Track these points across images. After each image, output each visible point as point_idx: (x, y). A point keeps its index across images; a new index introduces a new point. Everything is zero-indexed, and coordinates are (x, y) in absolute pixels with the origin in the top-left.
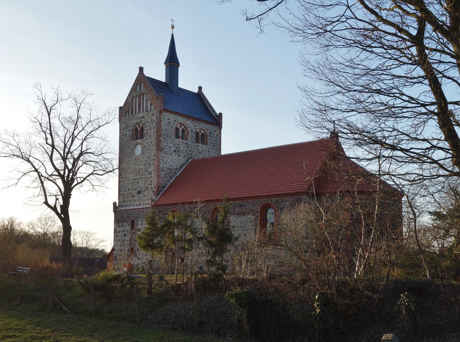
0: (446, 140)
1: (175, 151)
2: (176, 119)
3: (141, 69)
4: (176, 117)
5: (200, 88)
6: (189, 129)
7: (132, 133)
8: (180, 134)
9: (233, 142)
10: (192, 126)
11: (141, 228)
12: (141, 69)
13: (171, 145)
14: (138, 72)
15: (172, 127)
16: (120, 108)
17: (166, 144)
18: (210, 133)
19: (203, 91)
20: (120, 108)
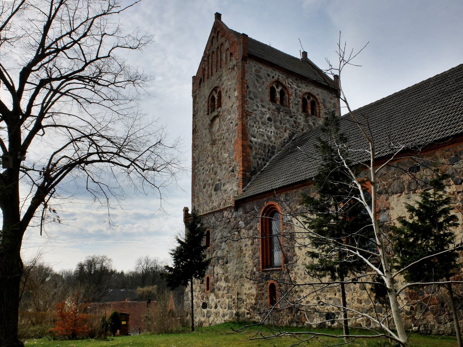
0: (355, 323)
1: (269, 119)
2: (269, 73)
3: (218, 16)
4: (270, 70)
5: (305, 54)
6: (291, 91)
7: (207, 99)
8: (278, 96)
9: (358, 93)
10: (295, 86)
11: (269, 285)
12: (218, 16)
13: (264, 110)
14: (212, 20)
15: (263, 83)
16: (194, 77)
17: (255, 108)
18: (324, 100)
19: (309, 57)
20: (194, 77)
